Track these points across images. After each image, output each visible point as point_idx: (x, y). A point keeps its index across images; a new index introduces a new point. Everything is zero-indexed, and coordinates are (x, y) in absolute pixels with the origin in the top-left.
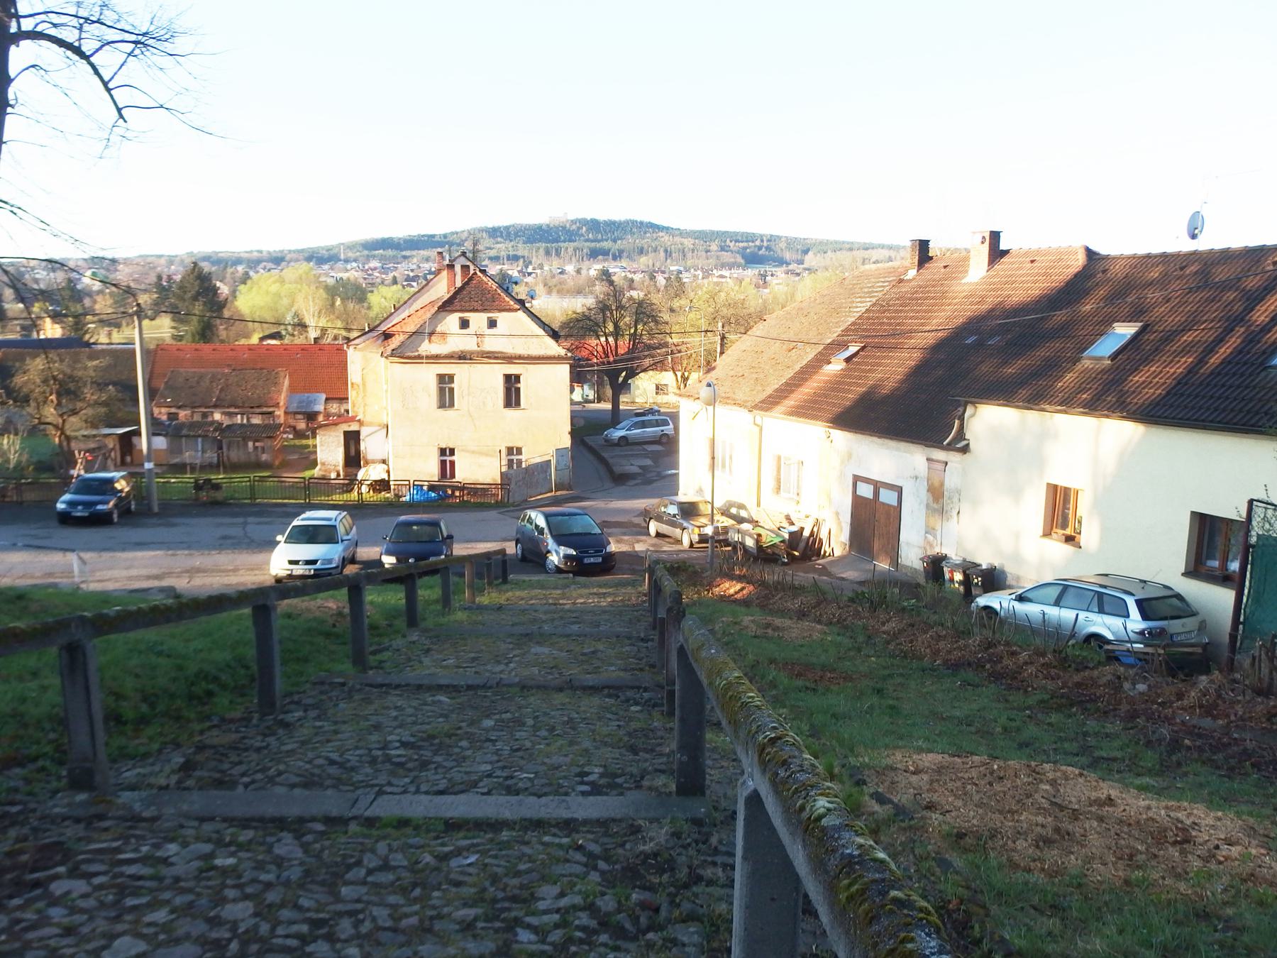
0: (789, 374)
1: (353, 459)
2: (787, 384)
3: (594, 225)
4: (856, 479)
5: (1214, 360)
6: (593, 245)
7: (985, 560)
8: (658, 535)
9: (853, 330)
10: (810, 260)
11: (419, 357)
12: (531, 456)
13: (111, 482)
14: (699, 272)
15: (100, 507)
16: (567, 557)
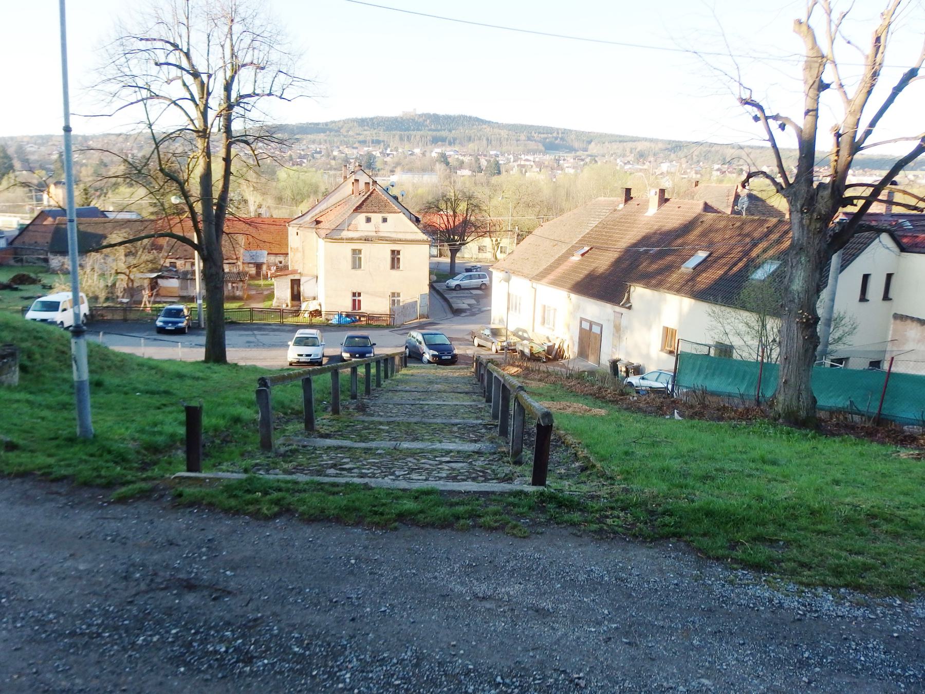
0: (552, 260)
1: (296, 296)
2: (550, 266)
3: (435, 118)
4: (582, 320)
5: (735, 269)
6: (434, 133)
7: (636, 361)
8: (479, 345)
9: (582, 242)
10: (593, 149)
11: (342, 239)
12: (405, 299)
13: (182, 310)
14: (511, 156)
15: (180, 325)
16: (433, 356)
